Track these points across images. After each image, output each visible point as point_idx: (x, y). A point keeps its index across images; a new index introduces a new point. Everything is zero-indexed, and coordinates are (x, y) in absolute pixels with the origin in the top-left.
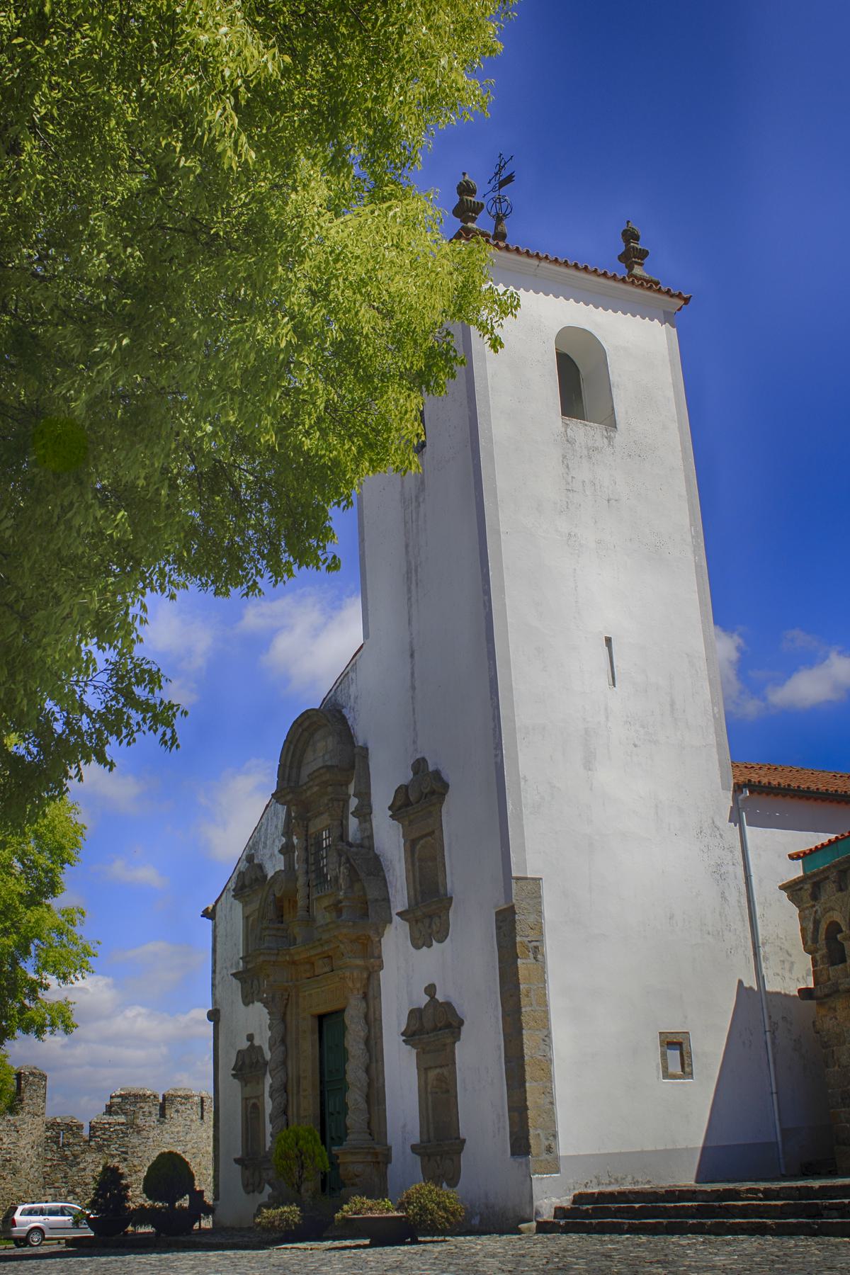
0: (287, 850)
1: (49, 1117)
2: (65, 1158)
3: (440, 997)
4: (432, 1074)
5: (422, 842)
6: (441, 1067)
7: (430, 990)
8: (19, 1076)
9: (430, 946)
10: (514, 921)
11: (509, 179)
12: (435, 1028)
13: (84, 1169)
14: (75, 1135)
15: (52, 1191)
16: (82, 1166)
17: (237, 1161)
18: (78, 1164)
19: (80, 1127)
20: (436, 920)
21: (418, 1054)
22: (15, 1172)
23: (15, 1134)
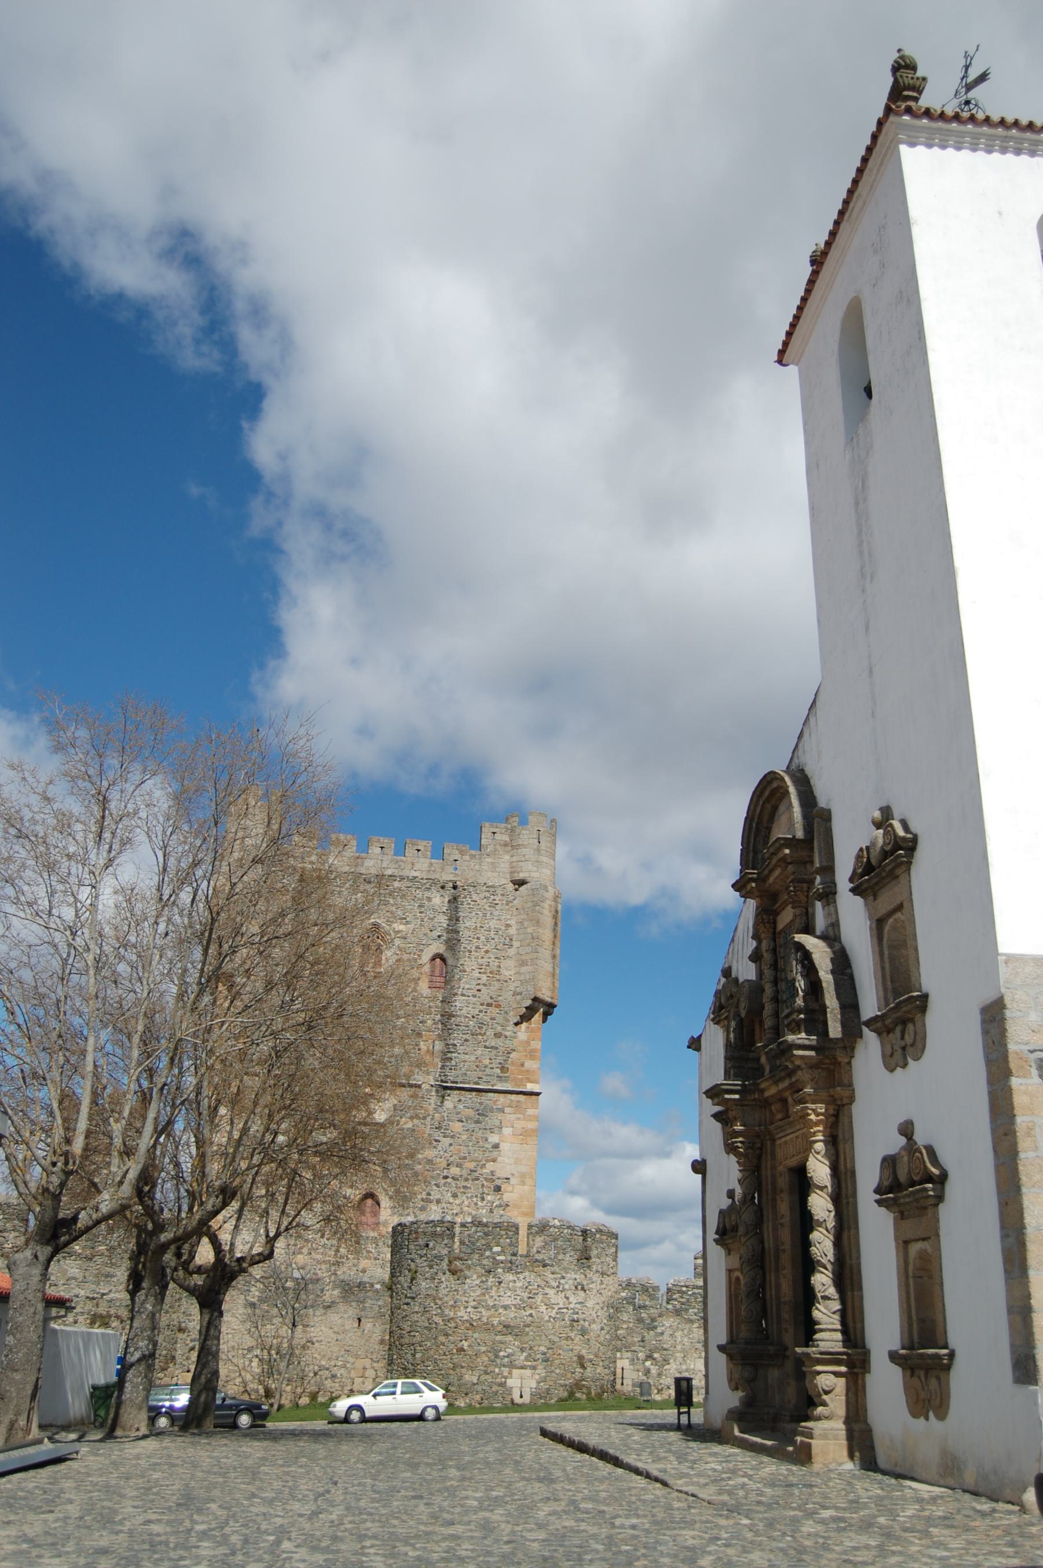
0: (756, 957)
1: (623, 1275)
2: (640, 1320)
3: (921, 1138)
4: (915, 1248)
5: (891, 920)
6: (924, 1239)
7: (907, 1130)
8: (585, 1232)
9: (905, 1066)
10: (1003, 1020)
11: (983, 78)
12: (914, 1185)
13: (662, 1334)
14: (652, 1297)
15: (629, 1355)
16: (659, 1330)
17: (721, 1348)
18: (655, 1327)
19: (656, 1289)
20: (910, 1027)
21: (895, 1219)
22: (583, 1332)
23: (582, 1293)
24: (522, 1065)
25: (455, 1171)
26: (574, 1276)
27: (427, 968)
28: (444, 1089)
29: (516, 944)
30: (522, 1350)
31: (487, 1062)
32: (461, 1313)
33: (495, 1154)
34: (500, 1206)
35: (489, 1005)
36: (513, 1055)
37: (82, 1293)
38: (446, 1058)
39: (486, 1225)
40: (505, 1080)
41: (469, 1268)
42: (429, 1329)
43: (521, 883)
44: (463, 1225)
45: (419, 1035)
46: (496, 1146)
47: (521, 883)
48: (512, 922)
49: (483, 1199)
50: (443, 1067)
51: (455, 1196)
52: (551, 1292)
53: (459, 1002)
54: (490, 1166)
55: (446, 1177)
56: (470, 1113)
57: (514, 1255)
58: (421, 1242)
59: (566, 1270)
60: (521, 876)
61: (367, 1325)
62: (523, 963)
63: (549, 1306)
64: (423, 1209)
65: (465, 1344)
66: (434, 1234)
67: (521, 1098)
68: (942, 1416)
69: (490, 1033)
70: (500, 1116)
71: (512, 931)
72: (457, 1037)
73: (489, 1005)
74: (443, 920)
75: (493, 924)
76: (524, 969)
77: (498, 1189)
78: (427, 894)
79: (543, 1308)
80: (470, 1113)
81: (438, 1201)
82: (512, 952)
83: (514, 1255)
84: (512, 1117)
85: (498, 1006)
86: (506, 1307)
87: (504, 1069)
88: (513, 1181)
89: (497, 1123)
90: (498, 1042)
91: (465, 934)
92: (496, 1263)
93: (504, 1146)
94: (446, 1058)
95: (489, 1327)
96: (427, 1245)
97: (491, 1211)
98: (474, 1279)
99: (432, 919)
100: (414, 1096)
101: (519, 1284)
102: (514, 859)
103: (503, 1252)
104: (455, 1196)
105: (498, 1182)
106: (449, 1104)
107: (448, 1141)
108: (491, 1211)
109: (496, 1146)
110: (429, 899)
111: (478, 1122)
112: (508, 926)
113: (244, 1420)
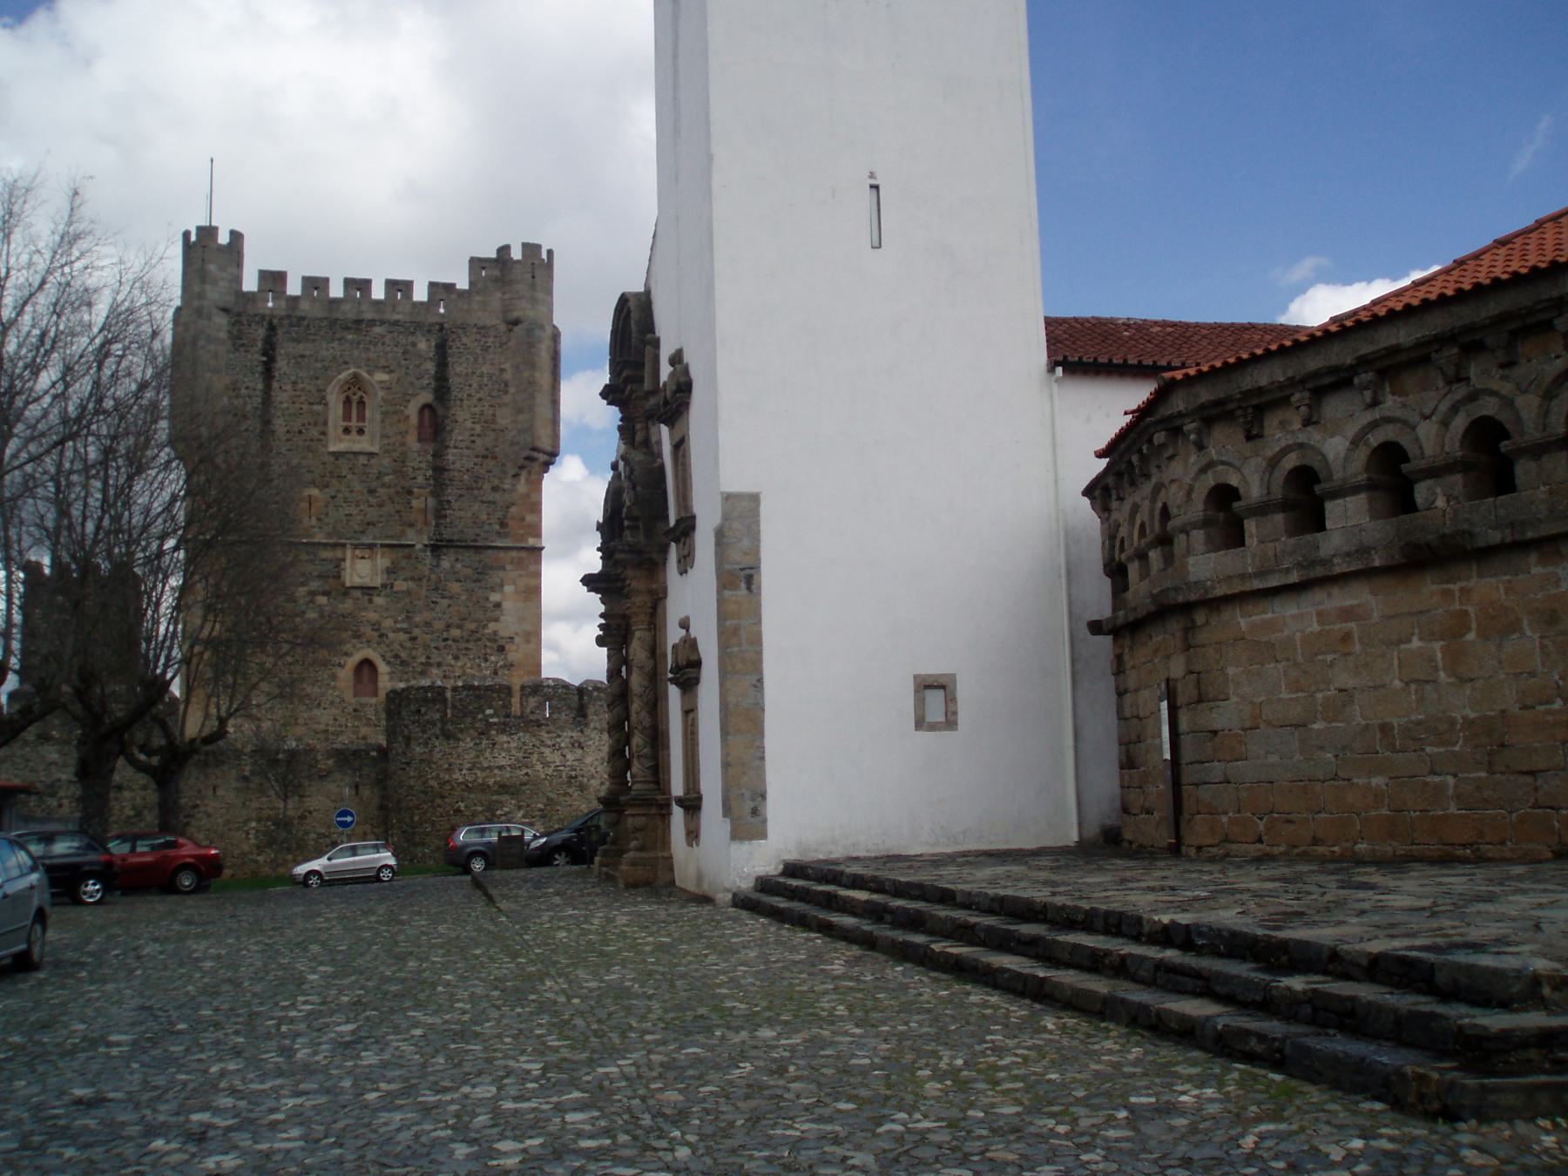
22: (582, 788)
24: (523, 519)
25: (456, 632)
26: (571, 734)
27: (414, 420)
28: (436, 548)
29: (512, 390)
30: (520, 808)
31: (484, 517)
32: (456, 775)
33: (497, 613)
34: (505, 666)
35: (485, 457)
36: (513, 510)
37: (64, 777)
38: (440, 514)
39: (478, 688)
40: (506, 536)
41: (461, 731)
42: (425, 793)
43: (516, 322)
44: (455, 689)
45: (410, 492)
46: (498, 605)
47: (516, 322)
48: (507, 366)
49: (486, 660)
50: (437, 526)
51: (456, 658)
52: (547, 751)
53: (451, 455)
54: (492, 626)
55: (446, 640)
56: (469, 572)
57: (508, 716)
58: (413, 708)
59: (562, 729)
60: (516, 314)
61: (366, 792)
62: (520, 411)
63: (546, 764)
64: (423, 673)
65: (462, 805)
66: (426, 700)
67: (523, 554)
68: (763, 835)
69: (487, 486)
70: (501, 574)
71: (508, 376)
72: (451, 493)
73: (485, 457)
74: (430, 367)
75: (485, 369)
76: (521, 417)
77: (501, 649)
78: (411, 339)
79: (539, 767)
80: (469, 572)
81: (439, 665)
82: (507, 399)
83: (508, 716)
84: (514, 574)
85: (495, 458)
86: (501, 768)
87: (503, 524)
88: (517, 640)
89: (498, 580)
90: (497, 496)
91: (454, 381)
92: (490, 726)
93: (507, 605)
94: (440, 514)
95: (484, 788)
96: (419, 711)
97: (496, 673)
98: (467, 743)
99: (418, 366)
100: (408, 557)
101: (513, 745)
102: (507, 296)
103: (495, 715)
104: (456, 658)
105: (502, 642)
106: (445, 564)
107: (445, 602)
108: (496, 673)
109: (498, 605)
110: (414, 345)
111: (478, 581)
112: (502, 370)
113: (186, 881)
